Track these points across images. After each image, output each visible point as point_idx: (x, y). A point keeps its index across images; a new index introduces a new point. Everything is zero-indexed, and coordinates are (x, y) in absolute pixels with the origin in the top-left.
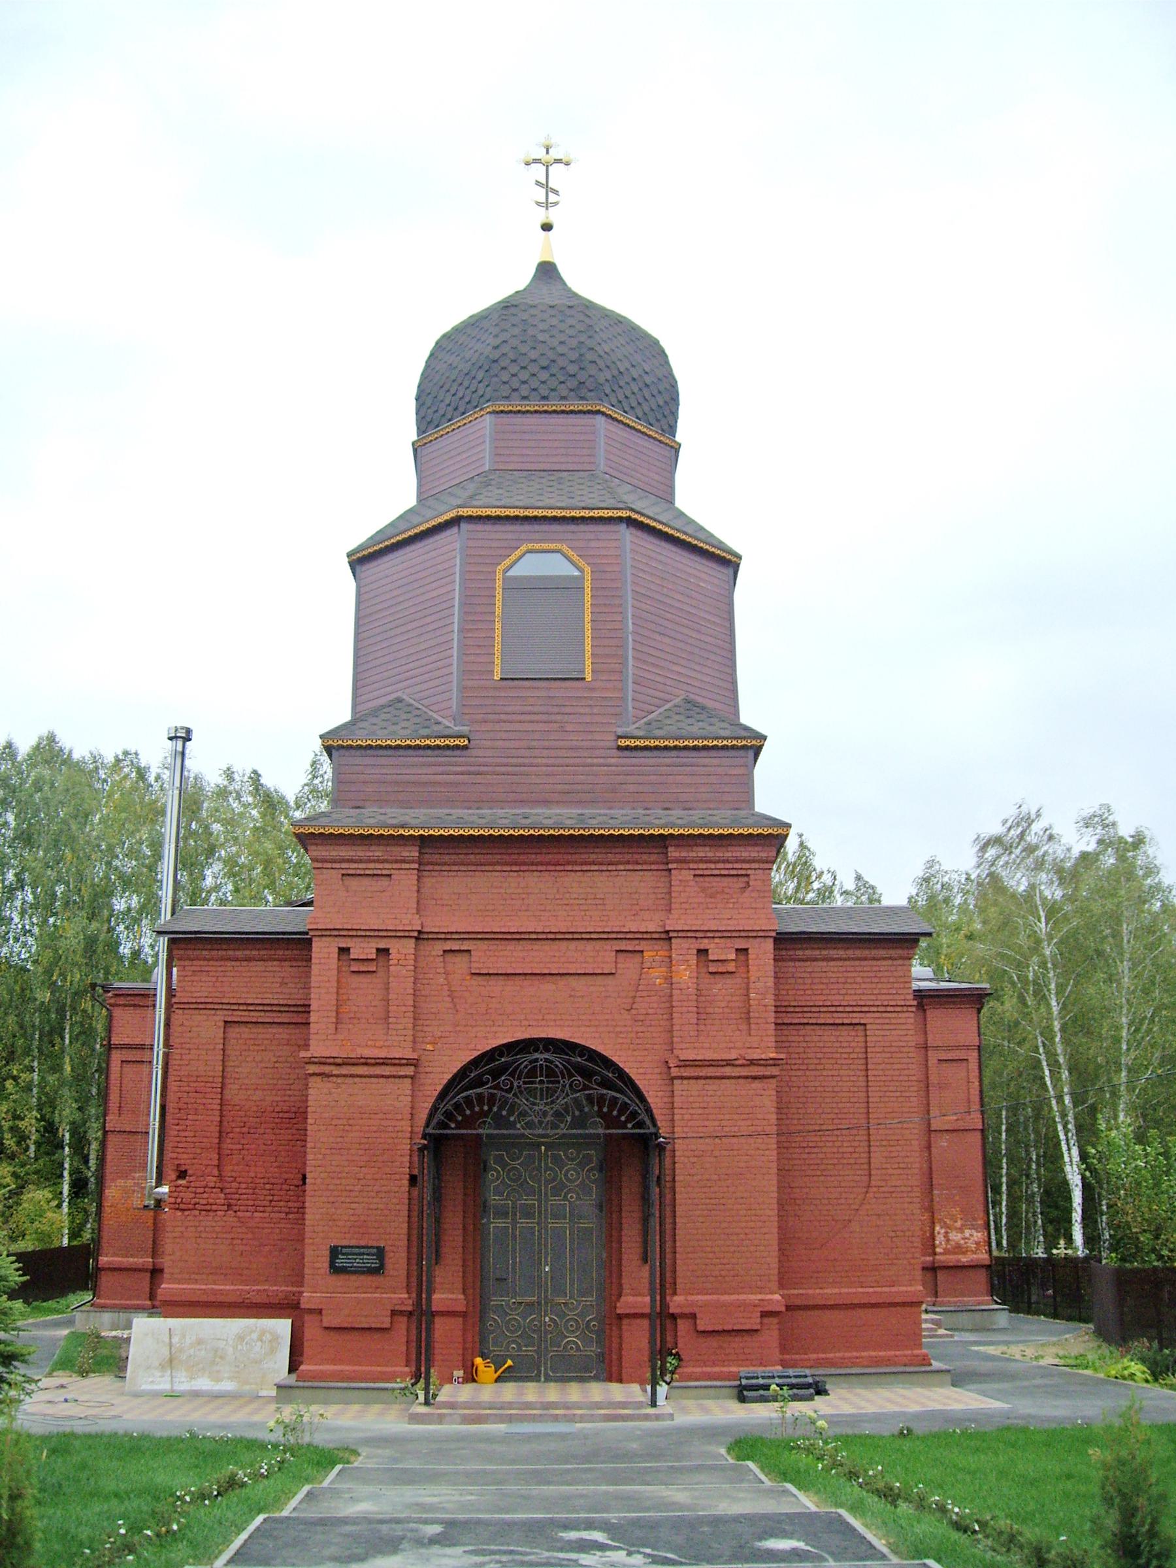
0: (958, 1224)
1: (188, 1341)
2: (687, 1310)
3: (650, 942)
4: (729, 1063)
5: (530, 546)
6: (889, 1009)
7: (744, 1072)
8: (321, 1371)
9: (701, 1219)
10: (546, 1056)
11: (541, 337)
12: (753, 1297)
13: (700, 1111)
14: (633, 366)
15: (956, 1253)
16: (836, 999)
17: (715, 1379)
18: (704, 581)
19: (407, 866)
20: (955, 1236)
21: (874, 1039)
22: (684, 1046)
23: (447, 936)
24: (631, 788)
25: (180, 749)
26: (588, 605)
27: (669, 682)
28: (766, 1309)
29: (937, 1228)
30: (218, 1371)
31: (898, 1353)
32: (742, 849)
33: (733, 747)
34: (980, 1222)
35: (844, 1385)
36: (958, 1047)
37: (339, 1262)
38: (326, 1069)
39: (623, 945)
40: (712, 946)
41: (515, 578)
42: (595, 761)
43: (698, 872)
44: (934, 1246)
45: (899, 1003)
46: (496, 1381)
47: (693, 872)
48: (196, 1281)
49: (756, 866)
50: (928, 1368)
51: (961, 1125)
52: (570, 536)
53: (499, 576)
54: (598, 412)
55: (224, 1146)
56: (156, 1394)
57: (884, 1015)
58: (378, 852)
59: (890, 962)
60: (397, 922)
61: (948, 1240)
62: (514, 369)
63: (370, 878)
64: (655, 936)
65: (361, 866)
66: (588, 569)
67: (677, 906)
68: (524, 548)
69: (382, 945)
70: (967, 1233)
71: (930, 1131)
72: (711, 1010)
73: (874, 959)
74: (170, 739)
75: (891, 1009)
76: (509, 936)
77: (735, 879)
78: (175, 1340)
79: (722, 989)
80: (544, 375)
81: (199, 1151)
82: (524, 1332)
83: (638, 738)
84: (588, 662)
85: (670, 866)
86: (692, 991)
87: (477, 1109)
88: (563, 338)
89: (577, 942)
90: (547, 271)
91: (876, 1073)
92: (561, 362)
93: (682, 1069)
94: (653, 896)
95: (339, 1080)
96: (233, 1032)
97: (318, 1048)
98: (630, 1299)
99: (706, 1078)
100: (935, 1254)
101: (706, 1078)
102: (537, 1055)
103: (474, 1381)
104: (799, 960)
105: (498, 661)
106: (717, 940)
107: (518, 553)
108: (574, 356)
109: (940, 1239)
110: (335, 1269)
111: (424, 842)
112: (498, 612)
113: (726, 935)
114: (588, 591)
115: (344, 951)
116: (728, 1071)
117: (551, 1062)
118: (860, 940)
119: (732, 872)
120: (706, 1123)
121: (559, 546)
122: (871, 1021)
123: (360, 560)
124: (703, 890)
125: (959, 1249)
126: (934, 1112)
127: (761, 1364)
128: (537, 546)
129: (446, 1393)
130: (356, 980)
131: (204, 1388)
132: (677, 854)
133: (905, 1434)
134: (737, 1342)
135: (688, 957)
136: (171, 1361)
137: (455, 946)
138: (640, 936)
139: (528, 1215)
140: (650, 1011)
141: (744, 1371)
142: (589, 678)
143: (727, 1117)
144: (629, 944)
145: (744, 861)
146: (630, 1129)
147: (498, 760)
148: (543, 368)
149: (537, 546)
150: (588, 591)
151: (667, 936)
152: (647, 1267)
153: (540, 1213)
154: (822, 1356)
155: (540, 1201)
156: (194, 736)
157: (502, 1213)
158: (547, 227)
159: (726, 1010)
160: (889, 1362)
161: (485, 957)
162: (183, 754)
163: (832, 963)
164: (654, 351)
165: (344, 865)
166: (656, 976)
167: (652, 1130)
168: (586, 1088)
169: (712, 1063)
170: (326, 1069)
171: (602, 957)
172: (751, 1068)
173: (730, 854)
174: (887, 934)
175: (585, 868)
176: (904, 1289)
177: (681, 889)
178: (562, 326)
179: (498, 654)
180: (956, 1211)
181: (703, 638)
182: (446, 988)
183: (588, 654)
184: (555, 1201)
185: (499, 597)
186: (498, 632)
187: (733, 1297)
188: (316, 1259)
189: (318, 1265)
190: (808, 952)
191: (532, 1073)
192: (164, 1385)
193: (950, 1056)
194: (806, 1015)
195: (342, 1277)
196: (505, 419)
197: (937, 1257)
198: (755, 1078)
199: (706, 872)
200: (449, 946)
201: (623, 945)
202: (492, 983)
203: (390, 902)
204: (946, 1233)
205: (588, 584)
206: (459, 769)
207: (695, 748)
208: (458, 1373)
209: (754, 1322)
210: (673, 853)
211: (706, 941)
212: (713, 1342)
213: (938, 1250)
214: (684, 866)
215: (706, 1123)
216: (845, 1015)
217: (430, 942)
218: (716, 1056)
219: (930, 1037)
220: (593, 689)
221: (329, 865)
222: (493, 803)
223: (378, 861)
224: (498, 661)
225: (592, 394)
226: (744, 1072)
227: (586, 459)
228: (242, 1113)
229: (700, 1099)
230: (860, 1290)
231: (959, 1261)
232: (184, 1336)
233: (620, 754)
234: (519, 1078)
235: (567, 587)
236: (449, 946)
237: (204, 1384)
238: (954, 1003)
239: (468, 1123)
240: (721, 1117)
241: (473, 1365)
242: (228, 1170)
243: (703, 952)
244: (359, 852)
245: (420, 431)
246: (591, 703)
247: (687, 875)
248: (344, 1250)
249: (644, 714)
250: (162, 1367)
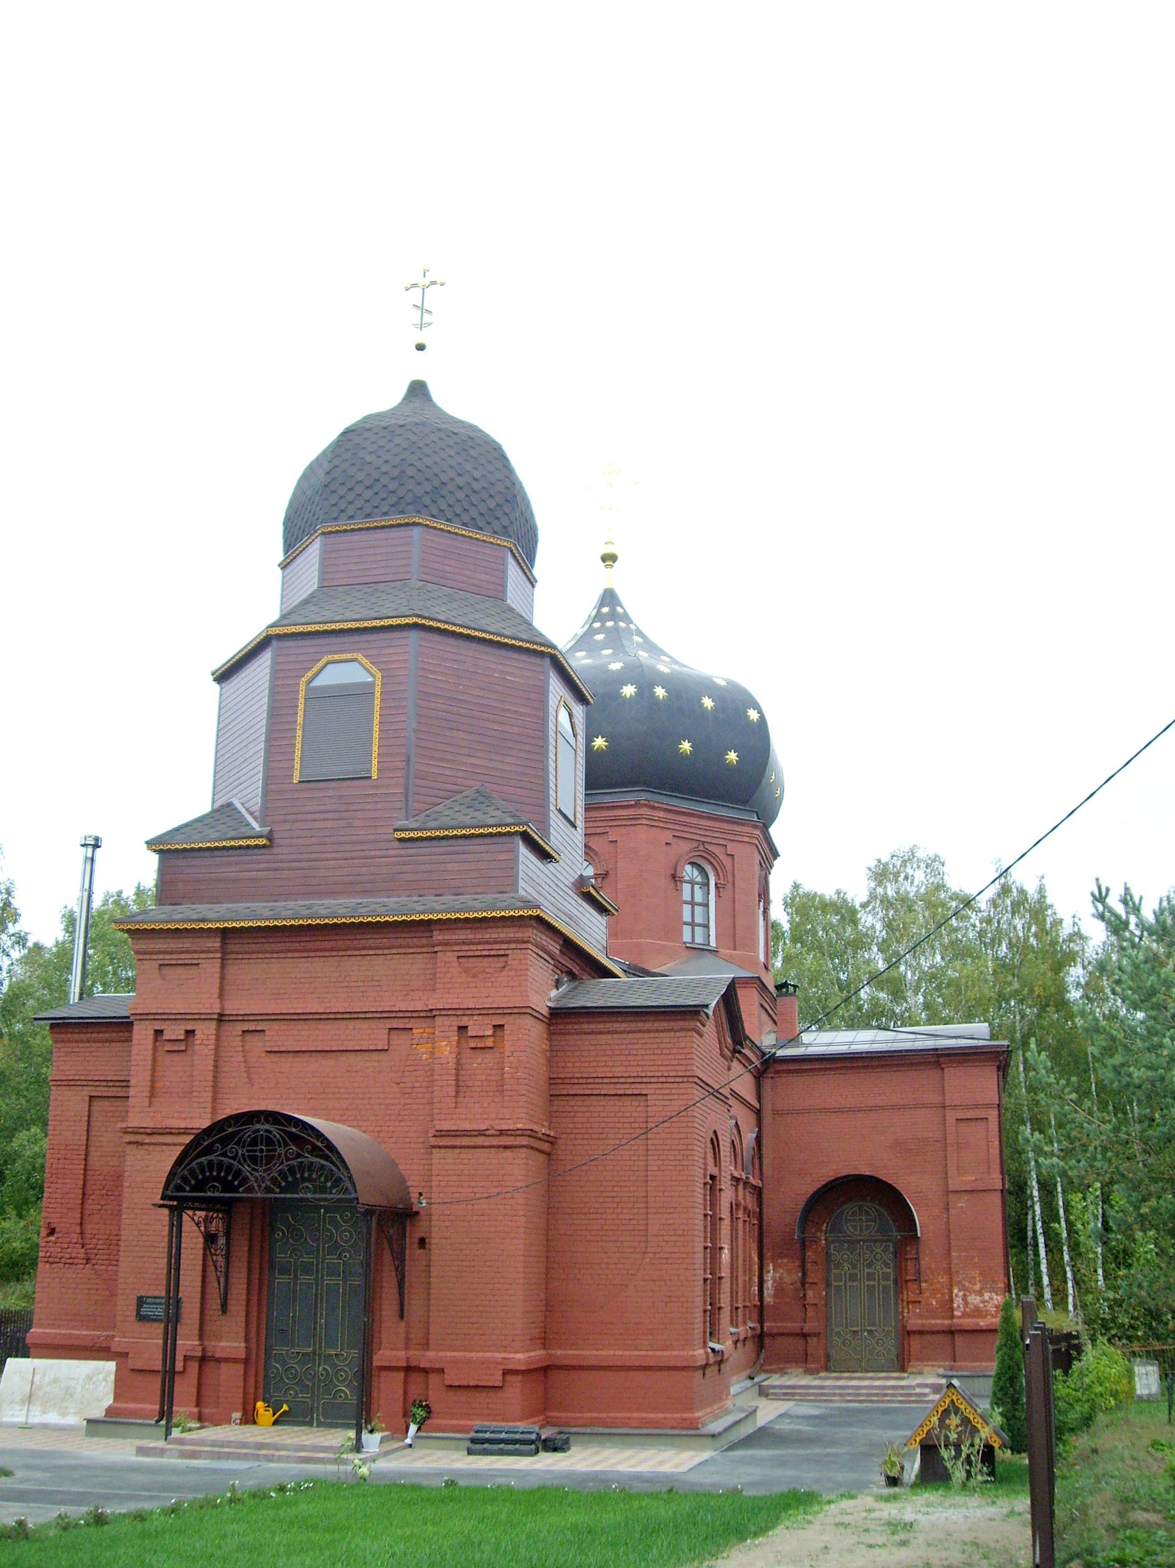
0: (977, 1287)
1: (47, 1380)
2: (437, 1366)
3: (418, 1020)
4: (481, 1133)
5: (330, 657)
6: (669, 1080)
7: (494, 1141)
8: (126, 1409)
9: (453, 1280)
10: (267, 1127)
11: (368, 458)
12: (497, 1355)
13: (456, 1178)
14: (460, 475)
15: (975, 1317)
16: (618, 1071)
17: (459, 1432)
18: (511, 674)
19: (211, 955)
20: (974, 1299)
21: (654, 1108)
22: (443, 1117)
23: (245, 1018)
24: (410, 877)
25: (89, 855)
26: (377, 708)
27: (459, 774)
28: (508, 1367)
29: (955, 1291)
30: (66, 1408)
31: (667, 1415)
32: (499, 930)
33: (499, 834)
34: (1001, 1285)
35: (608, 1444)
36: (976, 1106)
37: (144, 1311)
38: (139, 1138)
39: (395, 1024)
40: (471, 1023)
41: (317, 688)
42: (378, 853)
43: (461, 954)
44: (952, 1309)
45: (679, 1074)
46: (275, 1423)
47: (456, 954)
48: (59, 1327)
49: (513, 946)
50: (696, 1432)
51: (980, 1186)
52: (366, 645)
53: (302, 687)
54: (415, 524)
55: (86, 1206)
56: (13, 1426)
57: (666, 1085)
58: (186, 944)
59: (672, 1034)
60: (200, 1006)
61: (966, 1303)
62: (342, 491)
63: (182, 968)
64: (422, 1014)
65: (175, 956)
66: (379, 675)
67: (441, 986)
68: (324, 660)
69: (189, 1028)
70: (987, 1296)
71: (948, 1192)
72: (470, 1083)
73: (657, 1031)
74: (83, 845)
75: (672, 1080)
76: (296, 1017)
77: (496, 959)
78: (37, 1378)
79: (478, 1064)
80: (368, 494)
81: (65, 1211)
82: (301, 1380)
83: (412, 830)
84: (375, 762)
85: (436, 949)
86: (452, 1065)
87: (298, 1176)
88: (388, 457)
89: (356, 1022)
90: (418, 390)
91: (656, 1142)
92: (384, 481)
93: (438, 1139)
94: (422, 977)
95: (151, 1148)
96: (98, 1105)
97: (134, 1121)
98: (388, 1353)
99: (461, 1147)
100: (953, 1317)
101: (461, 1147)
102: (258, 1126)
103: (255, 1423)
104: (585, 1033)
105: (297, 766)
106: (475, 1018)
107: (320, 664)
108: (395, 473)
109: (958, 1302)
110: (142, 1318)
111: (225, 933)
112: (300, 720)
113: (484, 1012)
114: (378, 695)
115: (159, 1033)
116: (480, 1141)
117: (271, 1132)
118: (647, 1013)
119: (492, 953)
120: (460, 1190)
121: (355, 655)
122: (652, 1091)
123: (223, 676)
124: (466, 970)
125: (978, 1312)
126: (952, 1172)
127: (503, 1420)
128: (337, 657)
129: (176, 1433)
130: (169, 1058)
131: (53, 1421)
132: (441, 937)
133: (451, 1484)
134: (481, 1398)
135: (450, 1034)
136: (30, 1397)
137: (252, 1027)
138: (409, 1015)
139: (307, 1270)
140: (417, 1085)
141: (477, 1424)
142: (375, 776)
143: (480, 1184)
144: (399, 1022)
145: (502, 942)
146: (335, 1195)
147: (293, 857)
148: (367, 488)
149: (337, 657)
150: (378, 695)
151: (430, 1015)
152: (403, 1324)
153: (317, 1271)
154: (595, 1415)
155: (317, 1258)
156: (104, 844)
157: (285, 1271)
158: (420, 347)
159: (485, 1083)
160: (657, 1424)
161: (277, 1036)
162: (92, 860)
163: (615, 1036)
164: (495, 455)
165: (161, 956)
166: (423, 1051)
167: (353, 1195)
168: (299, 1156)
169: (466, 1133)
170: (139, 1138)
171: (375, 1034)
172: (501, 1138)
173: (488, 936)
174: (672, 1006)
175: (364, 952)
176: (676, 1353)
177: (444, 970)
178: (389, 446)
179: (297, 760)
180: (975, 1273)
181: (507, 728)
182: (243, 1065)
183: (375, 755)
184: (332, 1259)
185: (301, 706)
186: (299, 740)
187: (481, 1354)
188: (126, 1306)
189: (127, 1313)
190: (592, 1026)
191: (254, 1142)
192: (20, 1418)
193: (970, 1114)
194: (590, 1086)
195: (147, 1325)
196: (333, 539)
197: (955, 1320)
198: (505, 1147)
199: (469, 954)
200: (246, 1026)
201: (395, 1024)
202: (283, 1059)
203: (195, 990)
204: (965, 1295)
205: (378, 689)
206: (261, 866)
207: (464, 837)
208: (237, 1415)
209: (497, 1380)
210: (438, 936)
211: (466, 1018)
212: (461, 1396)
213: (956, 1313)
214: (449, 948)
215: (460, 1190)
216: (627, 1086)
217: (231, 1024)
218: (468, 1127)
219: (947, 1097)
220: (376, 787)
221: (148, 957)
222: (288, 896)
223: (187, 952)
224: (297, 766)
225: (410, 507)
226: (494, 1141)
227: (402, 570)
228: (101, 1178)
229: (456, 1167)
230: (636, 1353)
231: (978, 1324)
232: (44, 1375)
233: (403, 845)
234: (243, 1147)
235: (362, 692)
236: (246, 1026)
237: (53, 1418)
238: (973, 1061)
239: (292, 1187)
240: (474, 1184)
241: (254, 1408)
242: (88, 1228)
243: (462, 1029)
244: (173, 944)
245: (286, 552)
246: (377, 799)
247: (451, 956)
248: (149, 1300)
249: (427, 807)
250: (23, 1402)
